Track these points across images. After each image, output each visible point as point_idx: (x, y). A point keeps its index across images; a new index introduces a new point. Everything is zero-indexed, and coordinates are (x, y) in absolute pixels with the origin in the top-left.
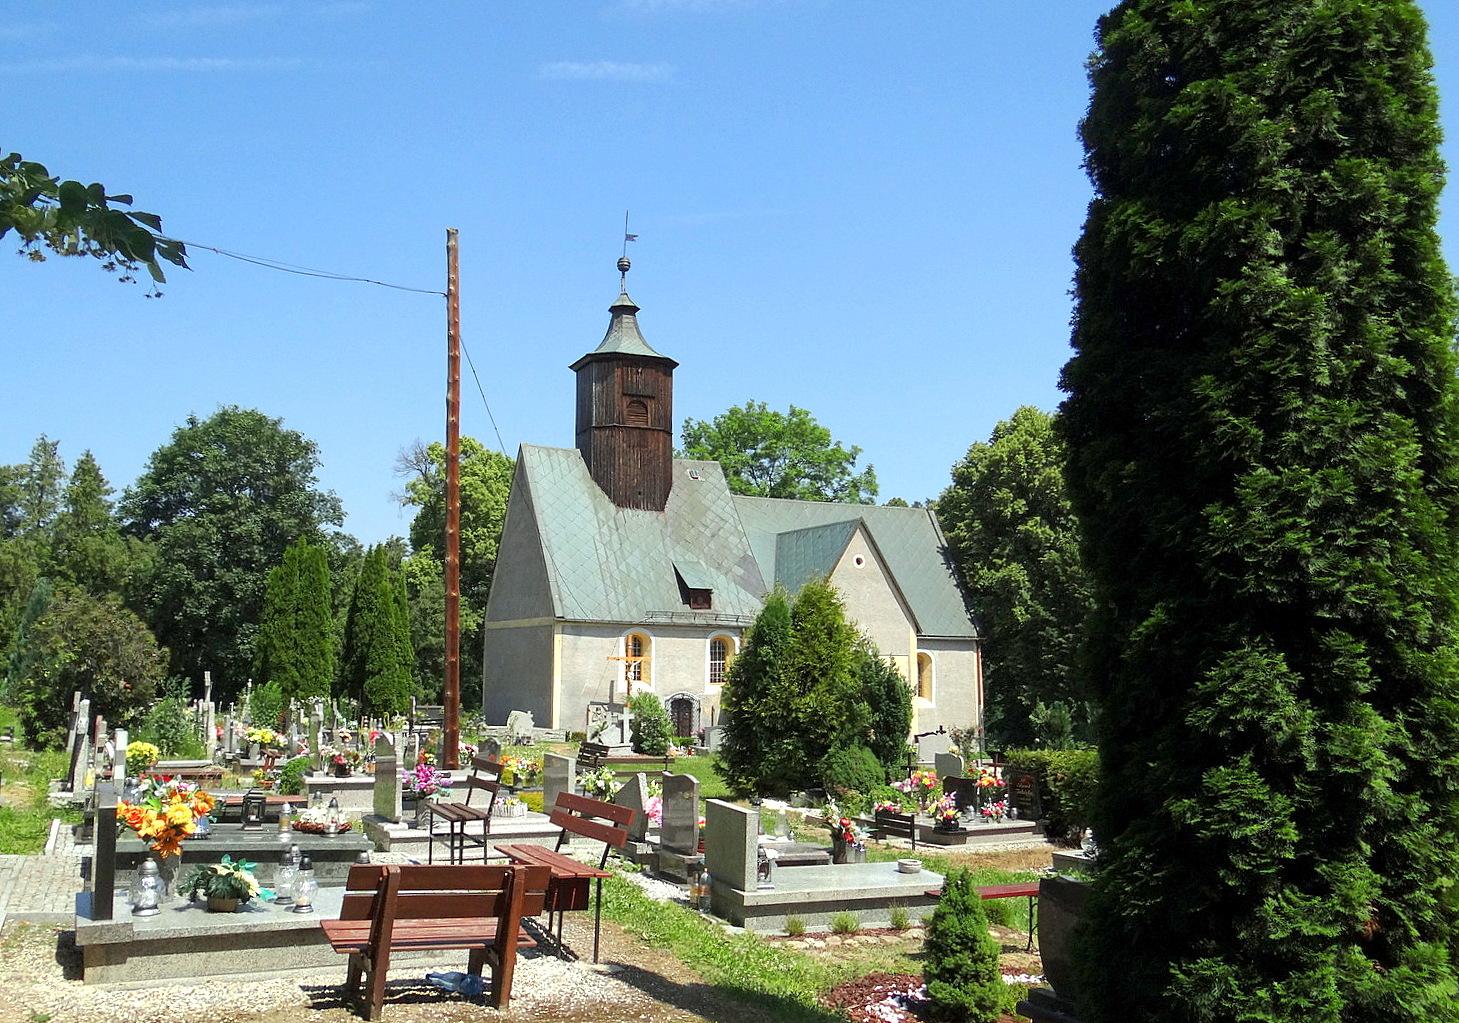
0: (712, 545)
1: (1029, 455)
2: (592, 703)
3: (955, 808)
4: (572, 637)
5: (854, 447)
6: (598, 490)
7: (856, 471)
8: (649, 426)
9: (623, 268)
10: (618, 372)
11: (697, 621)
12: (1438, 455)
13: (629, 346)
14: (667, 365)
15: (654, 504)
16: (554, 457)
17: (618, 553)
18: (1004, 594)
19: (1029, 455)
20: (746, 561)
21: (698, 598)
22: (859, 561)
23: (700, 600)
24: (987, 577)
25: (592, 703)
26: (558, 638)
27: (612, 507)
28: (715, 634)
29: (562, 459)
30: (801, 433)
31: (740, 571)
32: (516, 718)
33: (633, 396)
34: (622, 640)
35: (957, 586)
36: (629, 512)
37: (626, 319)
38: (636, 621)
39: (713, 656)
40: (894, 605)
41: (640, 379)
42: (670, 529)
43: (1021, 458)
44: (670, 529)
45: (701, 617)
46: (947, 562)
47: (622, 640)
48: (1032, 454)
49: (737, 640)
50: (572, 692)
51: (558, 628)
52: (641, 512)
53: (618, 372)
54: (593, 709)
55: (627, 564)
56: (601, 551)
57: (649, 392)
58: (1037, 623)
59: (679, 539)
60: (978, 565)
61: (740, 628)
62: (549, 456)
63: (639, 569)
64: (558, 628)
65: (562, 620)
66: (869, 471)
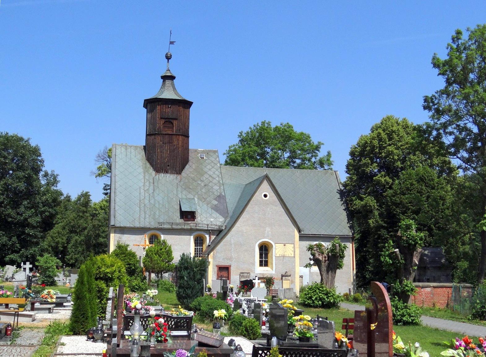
0: (204, 190)
1: (380, 140)
3: (257, 321)
5: (319, 143)
6: (148, 165)
7: (322, 154)
8: (174, 133)
9: (168, 58)
10: (158, 107)
11: (186, 227)
13: (168, 94)
14: (187, 104)
15: (176, 171)
16: (129, 150)
17: (151, 195)
18: (366, 212)
19: (380, 140)
20: (221, 198)
21: (188, 216)
22: (265, 196)
23: (189, 216)
24: (358, 204)
27: (154, 173)
28: (196, 233)
29: (133, 151)
30: (285, 136)
31: (215, 202)
32: (8, 269)
34: (192, 237)
35: (345, 210)
36: (162, 175)
37: (168, 82)
38: (152, 227)
39: (196, 244)
40: (295, 218)
41: (169, 111)
42: (182, 183)
43: (376, 142)
44: (182, 183)
45: (191, 225)
46: (341, 198)
47: (192, 237)
48: (381, 140)
49: (207, 236)
51: (113, 230)
52: (168, 175)
53: (158, 107)
55: (155, 200)
56: (143, 194)
57: (174, 117)
58: (379, 227)
59: (187, 188)
60: (354, 198)
61: (209, 230)
62: (126, 149)
63: (161, 202)
65: (114, 227)
66: (329, 154)
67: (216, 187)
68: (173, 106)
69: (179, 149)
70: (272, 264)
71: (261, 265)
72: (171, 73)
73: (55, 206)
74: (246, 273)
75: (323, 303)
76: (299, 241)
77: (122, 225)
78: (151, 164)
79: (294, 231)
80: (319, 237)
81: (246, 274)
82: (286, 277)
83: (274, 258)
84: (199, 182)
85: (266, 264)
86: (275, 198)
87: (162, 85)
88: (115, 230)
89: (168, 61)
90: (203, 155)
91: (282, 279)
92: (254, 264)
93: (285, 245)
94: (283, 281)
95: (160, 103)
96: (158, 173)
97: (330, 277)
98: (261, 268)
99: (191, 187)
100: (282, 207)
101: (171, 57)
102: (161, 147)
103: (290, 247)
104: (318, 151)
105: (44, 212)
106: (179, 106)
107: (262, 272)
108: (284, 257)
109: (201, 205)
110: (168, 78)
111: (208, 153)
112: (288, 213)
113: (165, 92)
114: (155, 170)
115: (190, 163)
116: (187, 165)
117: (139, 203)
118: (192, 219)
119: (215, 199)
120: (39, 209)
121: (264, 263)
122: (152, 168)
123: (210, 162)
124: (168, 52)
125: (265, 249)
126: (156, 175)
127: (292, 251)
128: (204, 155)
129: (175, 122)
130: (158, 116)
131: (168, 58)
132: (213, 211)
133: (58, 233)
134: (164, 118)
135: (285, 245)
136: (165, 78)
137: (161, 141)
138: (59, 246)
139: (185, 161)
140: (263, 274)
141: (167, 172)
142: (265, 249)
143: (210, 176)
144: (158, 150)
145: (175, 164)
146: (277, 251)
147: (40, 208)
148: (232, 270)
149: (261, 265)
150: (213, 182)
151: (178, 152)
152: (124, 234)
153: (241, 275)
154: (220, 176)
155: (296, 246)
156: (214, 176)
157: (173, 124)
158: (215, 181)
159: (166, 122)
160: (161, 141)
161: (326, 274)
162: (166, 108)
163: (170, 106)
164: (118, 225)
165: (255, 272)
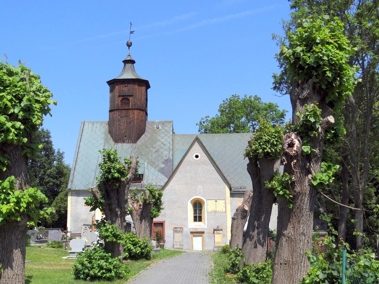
2: (84, 225)
4: (75, 197)
6: (109, 136)
8: (130, 107)
9: (129, 45)
10: (117, 87)
12: (16, 229)
14: (146, 84)
15: (132, 140)
16: (95, 125)
22: (197, 156)
25: (84, 225)
26: (69, 198)
27: (113, 142)
29: (98, 126)
31: (162, 166)
33: (123, 96)
37: (128, 65)
50: (75, 220)
52: (125, 144)
54: (84, 227)
57: (130, 94)
62: (93, 125)
64: (69, 194)
67: (166, 153)
68: (130, 85)
69: (134, 121)
70: (204, 219)
71: (195, 220)
72: (131, 57)
73: (60, 177)
74: (179, 228)
75: (130, 254)
76: (230, 197)
77: (77, 189)
78: (112, 136)
79: (225, 188)
80: (239, 193)
81: (179, 229)
82: (218, 231)
83: (206, 213)
84: (151, 149)
85: (200, 220)
86: (206, 158)
87: (123, 69)
88: (72, 193)
89: (129, 48)
90: (159, 126)
91: (214, 233)
92: (186, 219)
93: (216, 201)
94: (215, 235)
95: (118, 83)
96: (117, 143)
97: (143, 226)
98: (196, 223)
99: (143, 153)
100: (213, 166)
101: (131, 45)
102: (119, 120)
103: (221, 203)
104: (284, 118)
105: (49, 182)
106: (134, 85)
107: (195, 227)
108: (215, 212)
109: (149, 168)
110: (129, 62)
111: (163, 123)
112: (218, 171)
113: (124, 74)
114: (114, 141)
115: (146, 133)
116: (143, 135)
117: (95, 170)
118: (139, 181)
119: (163, 163)
120: (45, 180)
121: (198, 218)
122: (112, 139)
123: (165, 131)
124: (129, 40)
125: (198, 205)
126: (114, 145)
127: (224, 206)
128: (160, 125)
129: (131, 99)
130: (117, 94)
131: (129, 45)
132: (159, 173)
133: (61, 199)
134: (121, 96)
135: (216, 201)
136: (126, 62)
137: (119, 116)
138: (61, 209)
139: (141, 132)
140: (195, 229)
141: (124, 142)
142: (198, 205)
143: (162, 143)
144: (116, 123)
145: (131, 135)
146: (209, 207)
147: (45, 179)
148: (166, 225)
149: (195, 220)
150: (164, 148)
151: (134, 124)
152: (79, 196)
153: (175, 229)
154: (171, 143)
155: (227, 202)
156: (165, 143)
157: (129, 101)
158: (166, 147)
159: (122, 99)
160: (119, 116)
161: (139, 223)
162: (123, 87)
163: (126, 85)
164: (73, 189)
165: (187, 227)
